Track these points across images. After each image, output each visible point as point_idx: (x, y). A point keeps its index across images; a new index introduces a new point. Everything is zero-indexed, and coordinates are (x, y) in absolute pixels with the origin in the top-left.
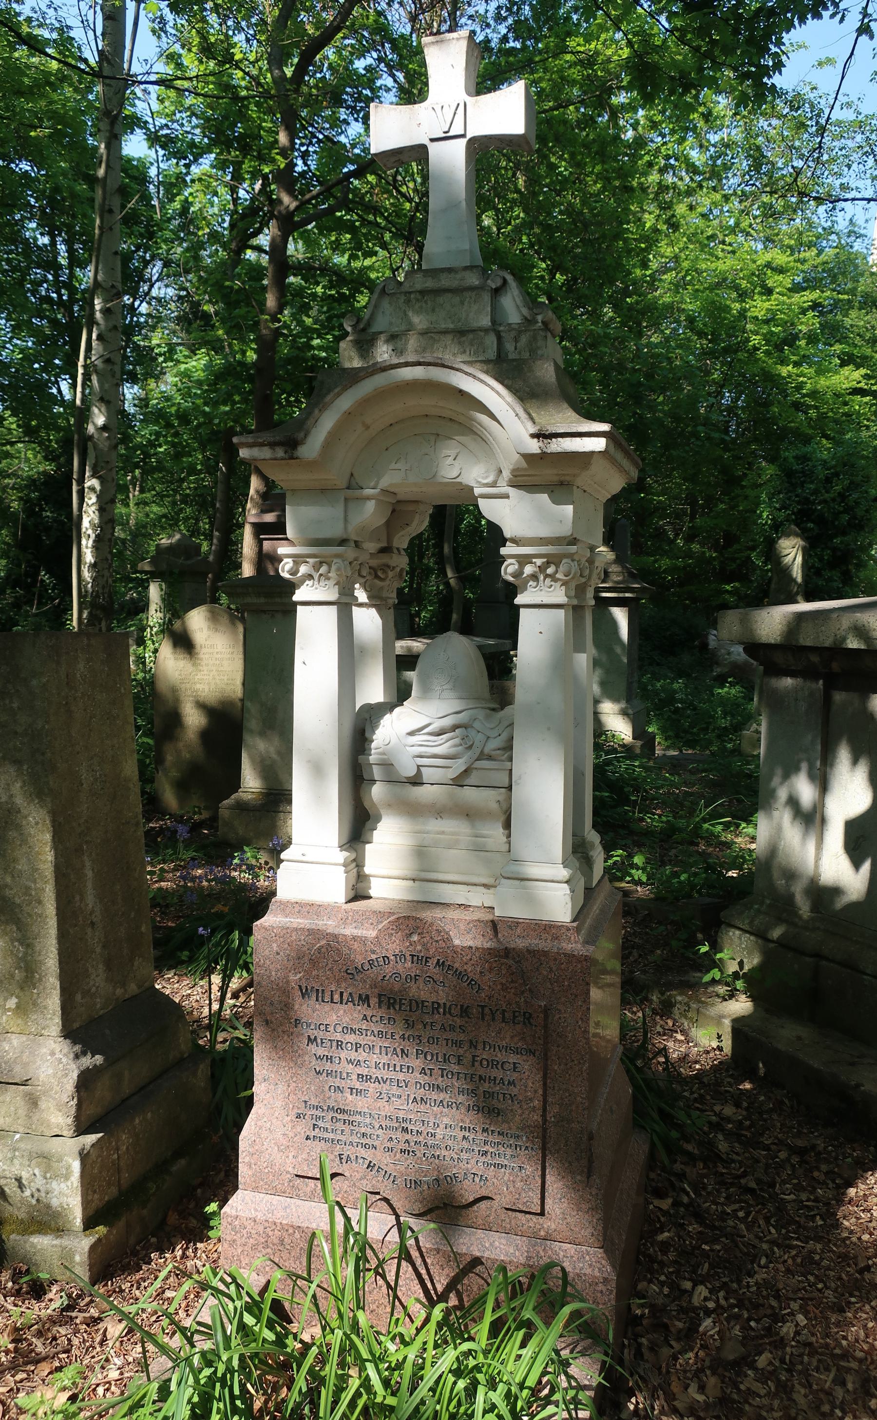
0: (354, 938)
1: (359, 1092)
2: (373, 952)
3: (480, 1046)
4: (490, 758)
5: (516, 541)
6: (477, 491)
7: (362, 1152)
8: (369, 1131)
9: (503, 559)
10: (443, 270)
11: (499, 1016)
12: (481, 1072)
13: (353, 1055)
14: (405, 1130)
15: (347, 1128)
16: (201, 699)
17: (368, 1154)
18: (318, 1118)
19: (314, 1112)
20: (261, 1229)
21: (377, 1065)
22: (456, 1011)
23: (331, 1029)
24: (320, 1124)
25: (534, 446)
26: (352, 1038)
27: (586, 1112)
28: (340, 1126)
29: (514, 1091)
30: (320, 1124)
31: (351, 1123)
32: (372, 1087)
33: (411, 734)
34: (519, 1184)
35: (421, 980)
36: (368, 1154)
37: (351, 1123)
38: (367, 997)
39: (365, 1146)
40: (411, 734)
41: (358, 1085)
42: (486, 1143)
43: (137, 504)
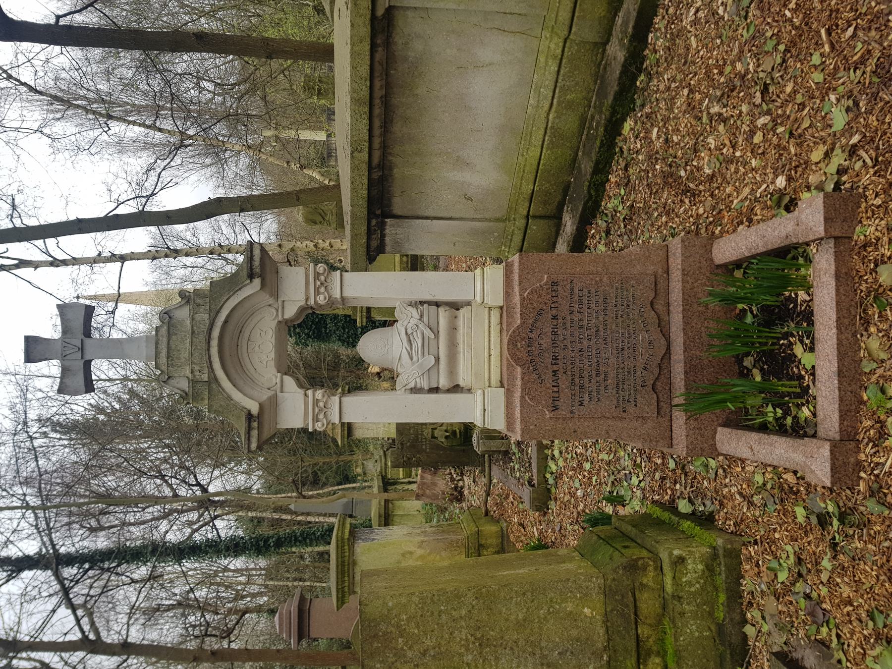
0: (522, 379)
1: (606, 376)
2: (529, 368)
4: (422, 316)
5: (307, 299)
6: (280, 318)
8: (626, 370)
11: (555, 299)
12: (585, 308)
13: (586, 379)
14: (623, 349)
15: (627, 383)
16: (399, 20)
20: (691, 432)
23: (573, 392)
24: (626, 398)
26: (577, 380)
28: (626, 387)
29: (593, 291)
30: (626, 398)
31: (624, 380)
32: (602, 369)
33: (411, 359)
34: (641, 287)
35: (541, 342)
36: (640, 370)
37: (624, 380)
40: (411, 359)
41: (602, 376)
43: (371, 253)
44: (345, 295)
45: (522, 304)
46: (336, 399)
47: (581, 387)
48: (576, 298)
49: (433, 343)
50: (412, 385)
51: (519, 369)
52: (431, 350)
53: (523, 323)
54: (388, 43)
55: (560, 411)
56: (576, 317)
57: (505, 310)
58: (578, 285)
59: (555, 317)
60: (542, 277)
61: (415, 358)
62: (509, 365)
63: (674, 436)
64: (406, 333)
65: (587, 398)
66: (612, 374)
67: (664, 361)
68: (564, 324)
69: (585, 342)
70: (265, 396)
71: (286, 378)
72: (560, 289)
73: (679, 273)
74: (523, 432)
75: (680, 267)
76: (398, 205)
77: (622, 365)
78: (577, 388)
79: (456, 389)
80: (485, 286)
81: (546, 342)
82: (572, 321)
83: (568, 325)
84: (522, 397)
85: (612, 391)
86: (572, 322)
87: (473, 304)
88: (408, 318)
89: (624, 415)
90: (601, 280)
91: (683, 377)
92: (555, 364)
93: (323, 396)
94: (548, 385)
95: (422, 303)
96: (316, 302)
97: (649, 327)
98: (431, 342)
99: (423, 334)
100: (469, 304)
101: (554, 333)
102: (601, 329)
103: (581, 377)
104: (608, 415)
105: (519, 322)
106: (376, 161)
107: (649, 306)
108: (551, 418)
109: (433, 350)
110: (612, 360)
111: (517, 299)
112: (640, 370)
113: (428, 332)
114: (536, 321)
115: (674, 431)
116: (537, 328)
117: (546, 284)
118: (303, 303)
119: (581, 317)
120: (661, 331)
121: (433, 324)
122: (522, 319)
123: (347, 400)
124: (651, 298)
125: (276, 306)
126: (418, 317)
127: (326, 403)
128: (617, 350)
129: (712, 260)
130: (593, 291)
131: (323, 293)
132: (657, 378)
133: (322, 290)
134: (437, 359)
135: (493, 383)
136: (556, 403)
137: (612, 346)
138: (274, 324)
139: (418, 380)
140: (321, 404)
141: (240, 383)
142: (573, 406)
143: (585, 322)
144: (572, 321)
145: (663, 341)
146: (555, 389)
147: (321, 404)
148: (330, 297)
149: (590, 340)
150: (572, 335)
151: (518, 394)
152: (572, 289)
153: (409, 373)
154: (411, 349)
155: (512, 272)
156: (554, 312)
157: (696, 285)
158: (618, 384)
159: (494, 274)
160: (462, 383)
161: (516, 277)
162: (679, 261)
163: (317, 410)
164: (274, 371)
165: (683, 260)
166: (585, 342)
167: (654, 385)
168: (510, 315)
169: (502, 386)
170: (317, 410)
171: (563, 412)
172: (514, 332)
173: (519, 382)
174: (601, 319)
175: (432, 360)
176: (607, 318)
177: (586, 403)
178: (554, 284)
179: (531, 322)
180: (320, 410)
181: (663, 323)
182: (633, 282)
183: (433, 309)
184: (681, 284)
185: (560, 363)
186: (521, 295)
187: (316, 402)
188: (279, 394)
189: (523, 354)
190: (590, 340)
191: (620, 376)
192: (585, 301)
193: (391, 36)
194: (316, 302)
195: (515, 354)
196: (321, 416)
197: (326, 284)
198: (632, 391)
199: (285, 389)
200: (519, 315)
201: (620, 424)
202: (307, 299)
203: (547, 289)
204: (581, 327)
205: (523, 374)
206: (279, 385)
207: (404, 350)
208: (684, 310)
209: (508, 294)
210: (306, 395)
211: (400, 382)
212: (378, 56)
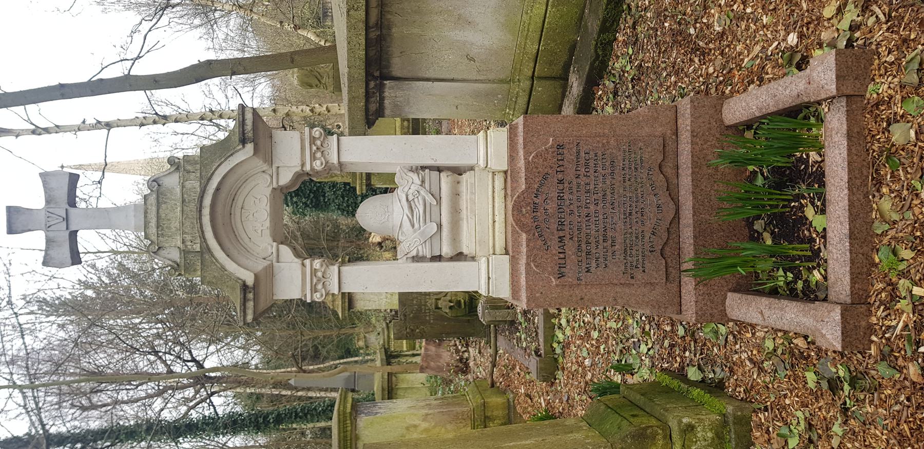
0: (528, 246)
1: (613, 241)
2: (534, 234)
3: (578, 173)
4: (423, 182)
5: (303, 165)
6: (275, 185)
7: (647, 238)
9: (313, 302)
10: (145, 217)
11: (561, 163)
13: (593, 245)
14: (630, 214)
17: (647, 235)
18: (632, 265)
19: (628, 268)
20: (701, 298)
21: (597, 231)
22: (561, 187)
23: (580, 259)
24: (634, 264)
25: (250, 147)
26: (584, 246)
27: (766, 365)
29: (600, 153)
30: (634, 264)
32: (610, 234)
33: (413, 226)
34: (649, 149)
36: (647, 235)
38: (560, 237)
39: (643, 237)
40: (413, 226)
41: (610, 242)
42: (630, 168)
44: (343, 159)
45: (526, 169)
46: (336, 268)
47: (588, 253)
48: (582, 161)
49: (435, 210)
51: (524, 236)
53: (528, 188)
55: (566, 279)
56: (583, 181)
57: (509, 175)
58: (584, 148)
59: (561, 182)
60: (548, 140)
61: (416, 226)
62: (514, 231)
64: (407, 200)
65: (594, 265)
66: (619, 240)
68: (570, 188)
69: (592, 207)
70: (260, 266)
72: (565, 152)
73: (688, 134)
75: (689, 128)
78: (584, 254)
79: (459, 257)
81: (552, 207)
82: (579, 185)
83: (575, 190)
84: (528, 264)
89: (632, 281)
90: (608, 142)
93: (322, 266)
95: (423, 168)
96: (312, 169)
97: (656, 191)
100: (472, 168)
101: (560, 198)
102: (608, 193)
103: (588, 243)
104: (615, 281)
105: (524, 187)
107: (657, 169)
108: (557, 286)
109: (435, 217)
110: (620, 225)
111: (521, 163)
113: (429, 198)
114: (541, 185)
116: (543, 193)
117: (552, 147)
118: (298, 169)
119: (587, 181)
121: (435, 190)
122: (526, 183)
126: (420, 183)
127: (324, 273)
128: (625, 214)
130: (600, 153)
131: (319, 159)
133: (319, 155)
134: (440, 226)
135: (498, 251)
136: (563, 270)
139: (420, 248)
140: (320, 274)
142: (580, 272)
143: (592, 187)
144: (579, 185)
145: (672, 205)
146: (562, 256)
147: (320, 274)
148: (327, 163)
151: (523, 261)
152: (578, 153)
155: (516, 135)
156: (560, 176)
157: (705, 146)
159: (498, 137)
161: (521, 140)
162: (688, 122)
163: (315, 280)
164: (270, 240)
166: (592, 207)
168: (515, 180)
169: (507, 253)
170: (315, 280)
171: (570, 279)
172: (518, 197)
173: (524, 249)
174: (608, 182)
176: (614, 181)
177: (593, 269)
178: (560, 147)
180: (319, 280)
181: (671, 187)
182: (641, 144)
183: (435, 174)
185: (567, 228)
186: (525, 159)
187: (314, 272)
188: (275, 264)
189: (528, 221)
192: (592, 164)
194: (312, 169)
196: (320, 286)
197: (322, 149)
199: (281, 259)
200: (523, 179)
201: (627, 290)
202: (303, 165)
204: (588, 192)
205: (528, 240)
207: (405, 217)
209: (512, 158)
210: (303, 265)
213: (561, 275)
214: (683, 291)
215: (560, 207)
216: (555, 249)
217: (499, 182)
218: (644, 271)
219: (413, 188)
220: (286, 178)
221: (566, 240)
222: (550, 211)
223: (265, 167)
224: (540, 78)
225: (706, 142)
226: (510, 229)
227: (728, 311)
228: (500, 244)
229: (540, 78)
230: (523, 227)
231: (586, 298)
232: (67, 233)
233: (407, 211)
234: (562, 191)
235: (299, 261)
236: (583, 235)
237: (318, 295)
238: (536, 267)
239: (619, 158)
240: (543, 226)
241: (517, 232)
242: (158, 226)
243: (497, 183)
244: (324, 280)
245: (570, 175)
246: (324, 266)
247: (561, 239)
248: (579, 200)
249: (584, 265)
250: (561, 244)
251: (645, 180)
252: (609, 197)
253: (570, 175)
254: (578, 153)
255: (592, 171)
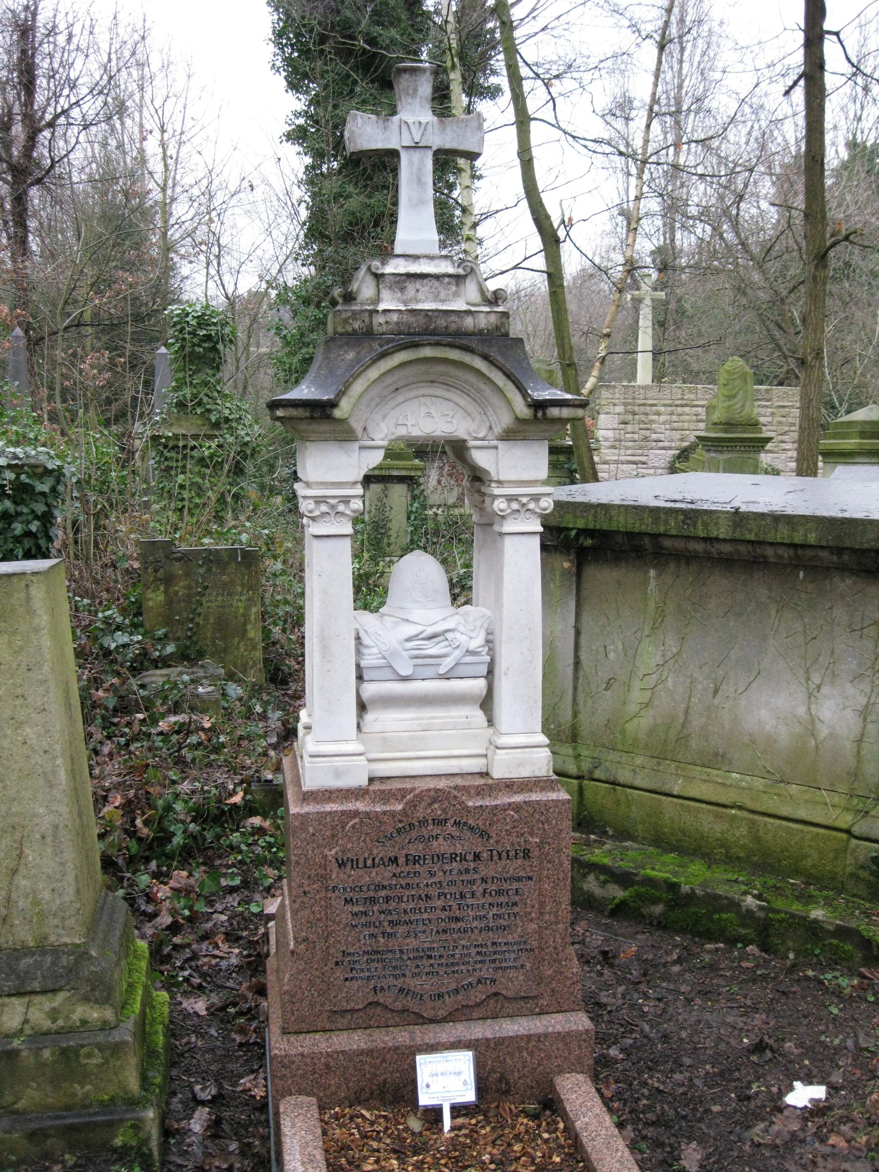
0: (384, 813)
2: (400, 821)
3: (489, 881)
6: (472, 443)
11: (504, 854)
13: (385, 906)
14: (430, 957)
15: (379, 965)
20: (308, 1060)
22: (470, 857)
24: (357, 966)
26: (383, 893)
30: (357, 966)
31: (383, 960)
32: (401, 930)
33: (409, 640)
34: (521, 978)
36: (399, 983)
37: (383, 960)
38: (396, 858)
40: (409, 640)
41: (389, 930)
42: (495, 953)
44: (508, 541)
47: (373, 900)
48: (505, 886)
49: (430, 671)
50: (366, 640)
51: (399, 807)
52: (420, 670)
54: (843, 569)
56: (479, 888)
58: (526, 887)
59: (477, 857)
61: (410, 645)
62: (403, 793)
63: (301, 1037)
65: (356, 909)
66: (393, 944)
67: (413, 1016)
68: (467, 871)
69: (440, 903)
70: (356, 425)
71: (381, 454)
72: (519, 861)
74: (302, 815)
75: (550, 1030)
76: (601, 576)
77: (405, 957)
78: (371, 894)
79: (362, 707)
80: (520, 748)
81: (441, 846)
82: (472, 882)
83: (465, 877)
84: (356, 813)
85: (368, 944)
86: (469, 882)
87: (491, 731)
88: (466, 627)
89: (331, 964)
91: (390, 1044)
92: (407, 860)
93: (354, 511)
94: (375, 852)
95: (492, 651)
96: (495, 497)
97: (462, 992)
98: (433, 668)
99: (446, 656)
100: (490, 722)
101: (453, 857)
102: (459, 924)
103: (387, 899)
105: (470, 804)
106: (667, 543)
110: (413, 943)
112: (399, 983)
113: (446, 665)
114: (472, 829)
115: (308, 1036)
119: (478, 894)
120: (457, 1010)
122: (476, 808)
123: (347, 544)
124: (504, 992)
125: (490, 437)
127: (342, 514)
128: (429, 949)
129: (560, 1072)
130: (516, 909)
131: (509, 506)
132: (386, 1007)
133: (515, 506)
137: (433, 941)
138: (461, 434)
139: (375, 650)
140: (341, 508)
141: (375, 391)
143: (470, 901)
144: (472, 882)
145: (442, 1013)
146: (369, 862)
148: (503, 517)
149: (444, 909)
150: (451, 883)
151: (360, 806)
152: (519, 879)
153: (386, 632)
154: (423, 639)
155: (542, 789)
157: (525, 1054)
158: (379, 952)
159: (538, 761)
160: (369, 717)
161: (535, 797)
162: (559, 1028)
163: (333, 501)
165: (559, 1033)
166: (440, 903)
167: (377, 1003)
168: (480, 792)
169: (371, 780)
171: (336, 876)
172: (455, 797)
175: (403, 673)
176: (476, 932)
177: (349, 907)
179: (470, 822)
180: (333, 507)
181: (467, 1011)
183: (484, 670)
184: (526, 1033)
186: (510, 804)
187: (346, 500)
188: (356, 445)
189: (420, 813)
190: (444, 909)
191: (390, 956)
192: (502, 899)
193: (852, 574)
194: (495, 497)
195: (422, 799)
196: (324, 508)
197: (522, 511)
198: (367, 974)
200: (478, 804)
202: (500, 483)
203: (519, 843)
205: (392, 814)
206: (371, 443)
207: (420, 628)
208: (487, 1040)
209: (510, 785)
210: (355, 483)
211: (367, 618)
212: (824, 554)
213: (341, 864)
214: (317, 1036)
215: (440, 857)
216: (380, 852)
217: (475, 765)
218: (346, 979)
219: (463, 639)
220: (481, 458)
221: (392, 868)
222: (435, 844)
223: (498, 430)
224: (581, 791)
225: (531, 1054)
226: (408, 785)
227: (291, 1099)
228: (383, 769)
229: (581, 791)
230: (413, 805)
231: (306, 900)
232: (398, 147)
233: (430, 631)
234: (463, 858)
235: (361, 478)
236: (399, 892)
237: (312, 506)
238: (353, 827)
239: (510, 937)
240: (414, 834)
241: (404, 797)
242: (410, 276)
243: (474, 761)
244: (333, 515)
245: (487, 870)
246: (354, 515)
247: (394, 860)
248: (451, 883)
249: (355, 896)
250: (386, 860)
251: (477, 974)
252: (453, 925)
253: (487, 870)
254: (519, 879)
255: (491, 900)
